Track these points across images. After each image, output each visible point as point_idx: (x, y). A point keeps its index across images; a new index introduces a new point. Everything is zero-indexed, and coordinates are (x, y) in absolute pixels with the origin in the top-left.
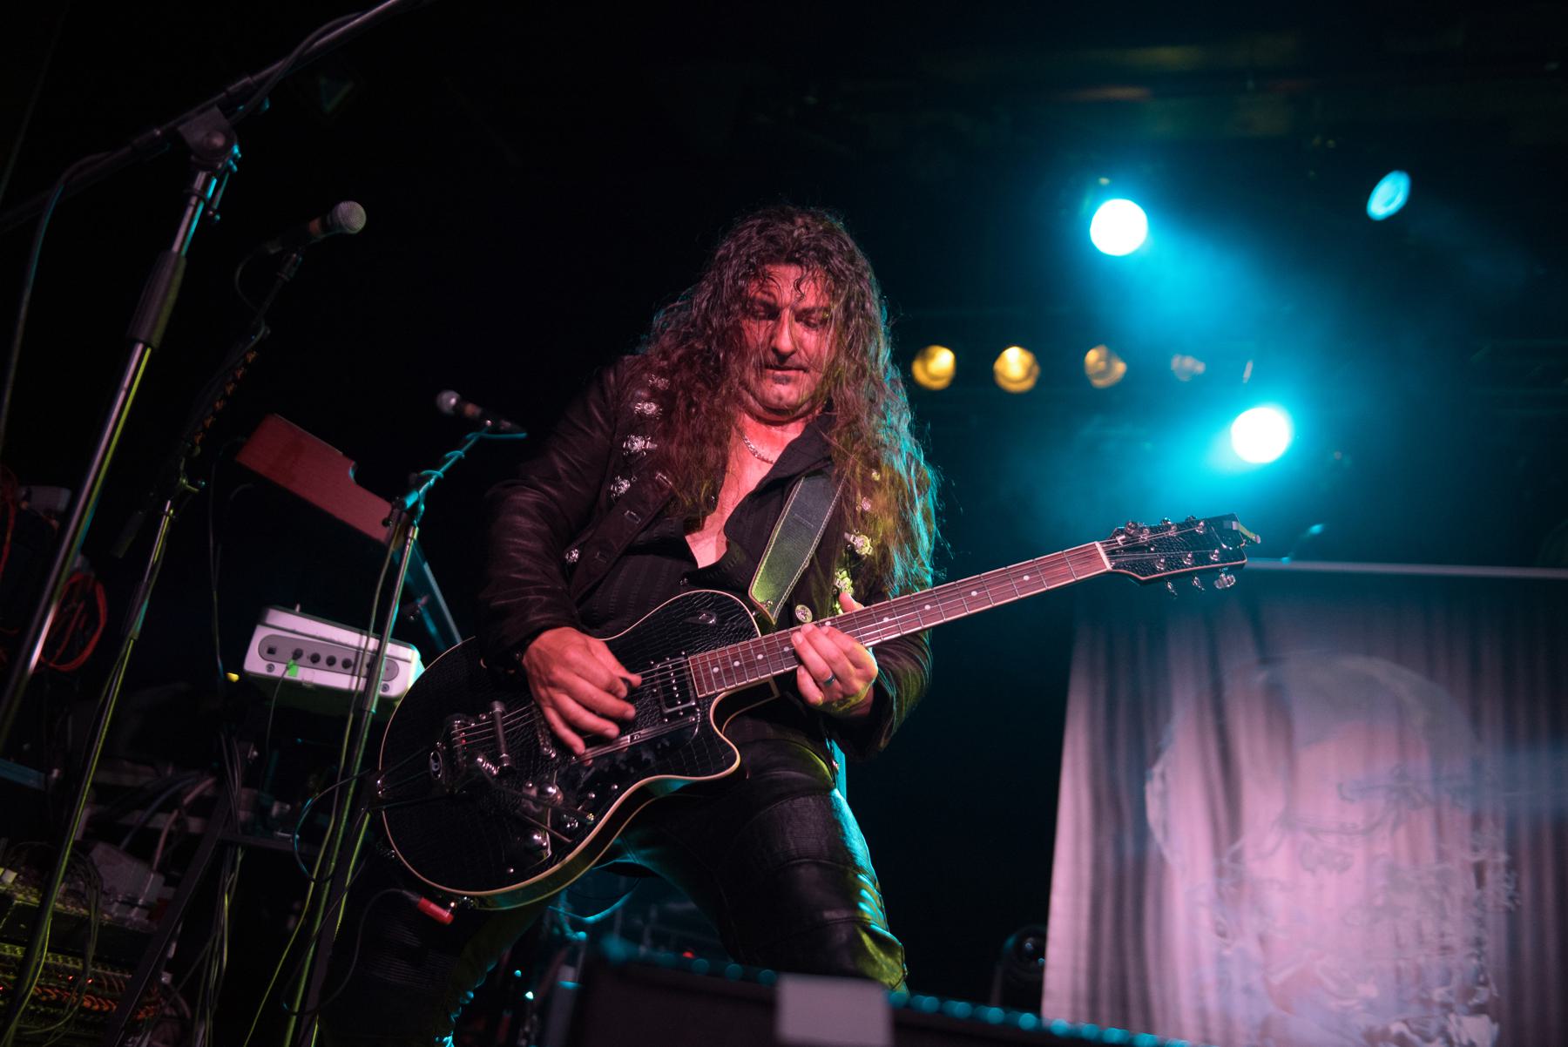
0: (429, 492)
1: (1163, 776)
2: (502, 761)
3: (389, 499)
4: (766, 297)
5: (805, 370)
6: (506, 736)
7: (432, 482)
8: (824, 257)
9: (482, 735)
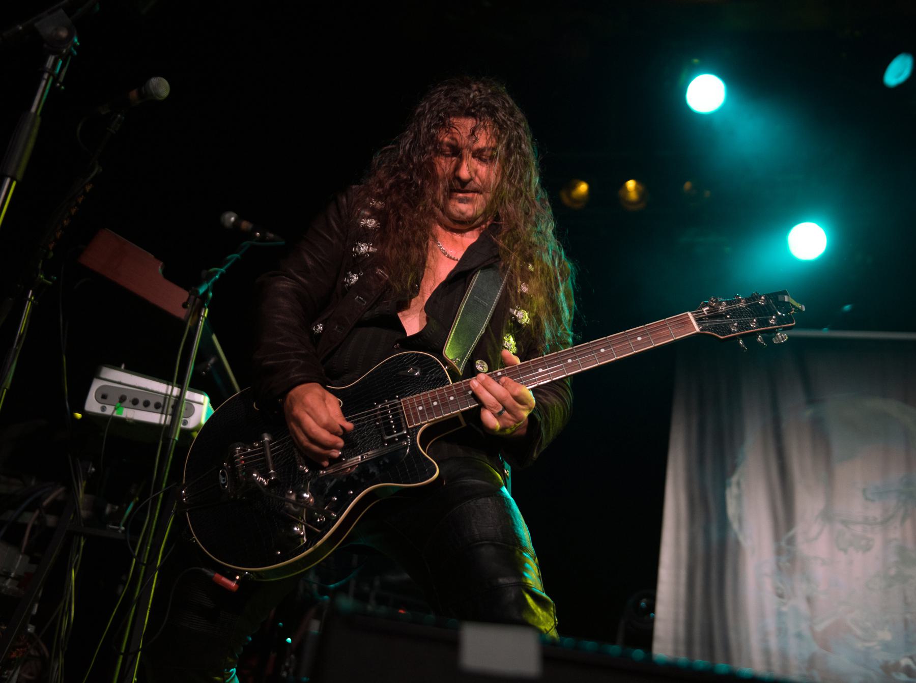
0: (215, 284)
2: (270, 475)
3: (187, 288)
6: (273, 458)
9: (255, 458)
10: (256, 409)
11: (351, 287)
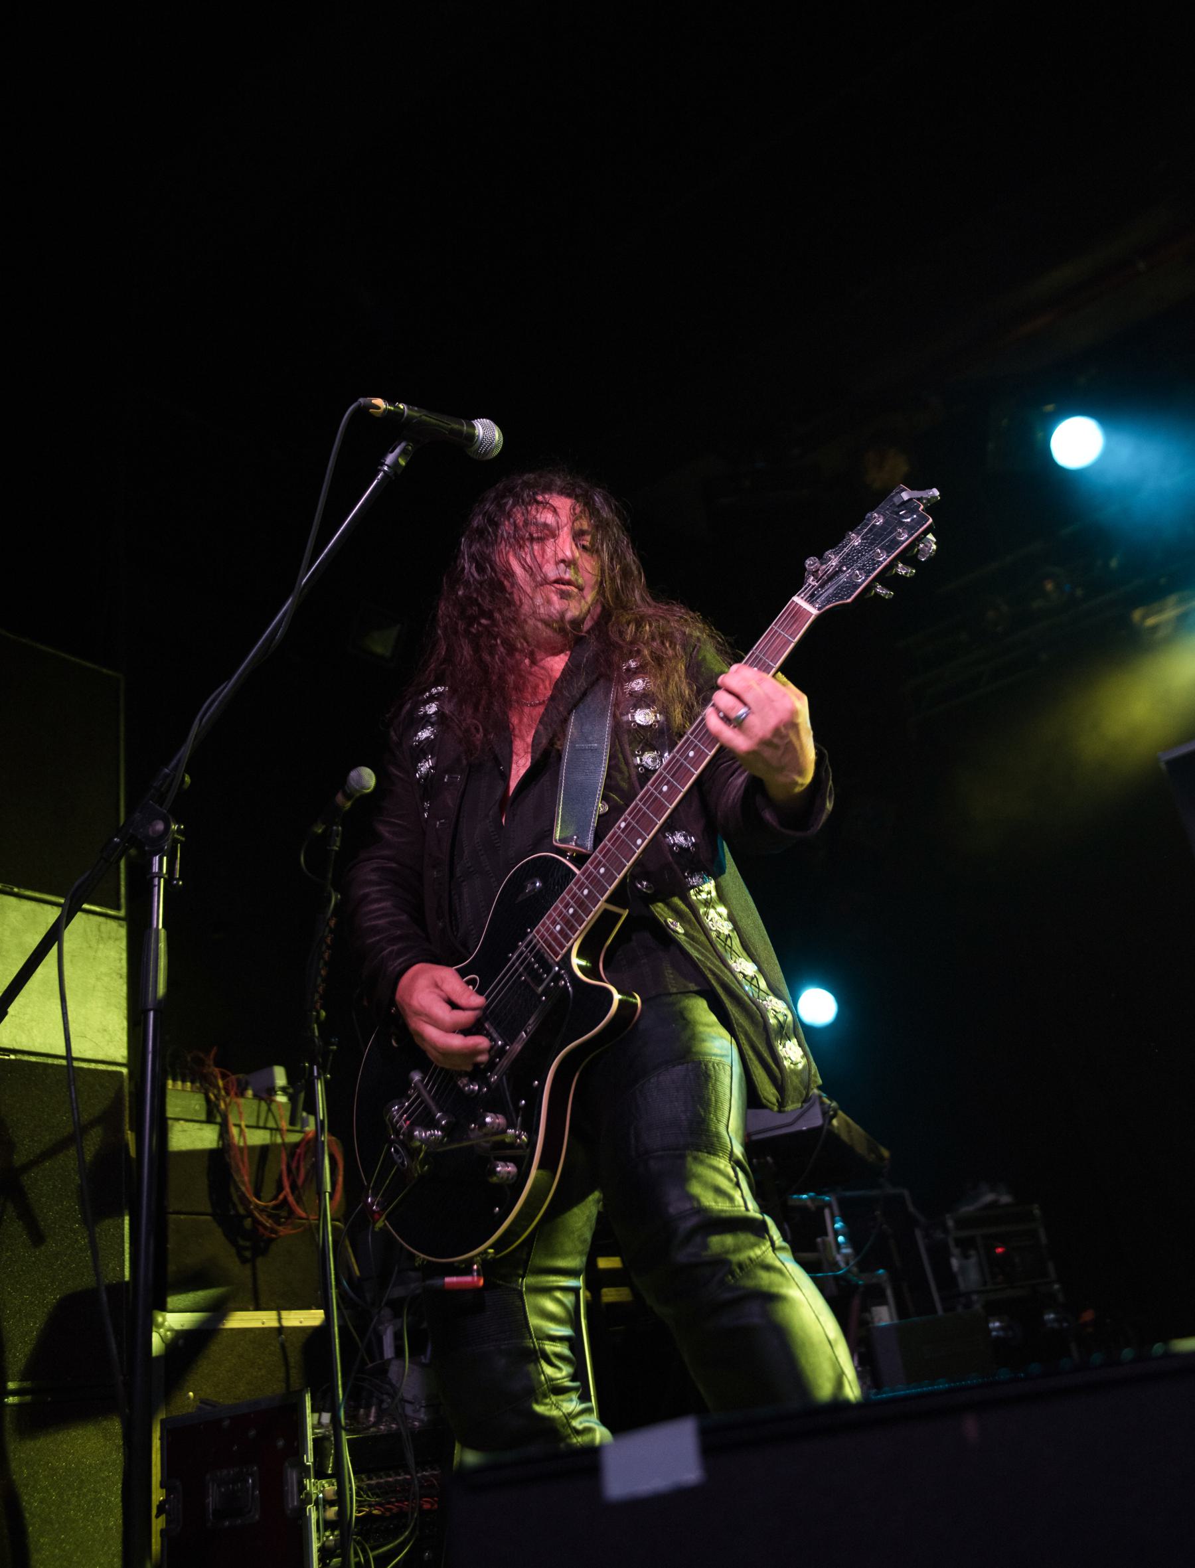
6: (433, 1098)
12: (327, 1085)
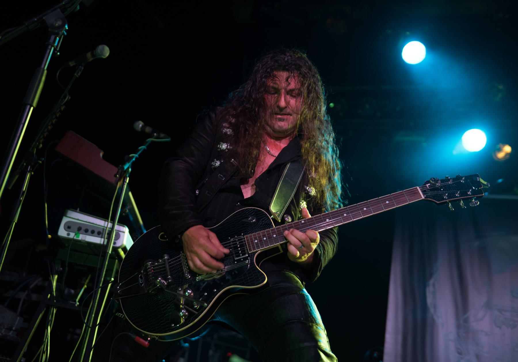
0: (133, 163)
1: (434, 285)
2: (168, 279)
3: (117, 166)
4: (275, 85)
5: (291, 115)
6: (170, 269)
7: (134, 159)
8: (298, 68)
9: (160, 268)
10: (160, 239)
11: (216, 168)
12: (31, 176)
